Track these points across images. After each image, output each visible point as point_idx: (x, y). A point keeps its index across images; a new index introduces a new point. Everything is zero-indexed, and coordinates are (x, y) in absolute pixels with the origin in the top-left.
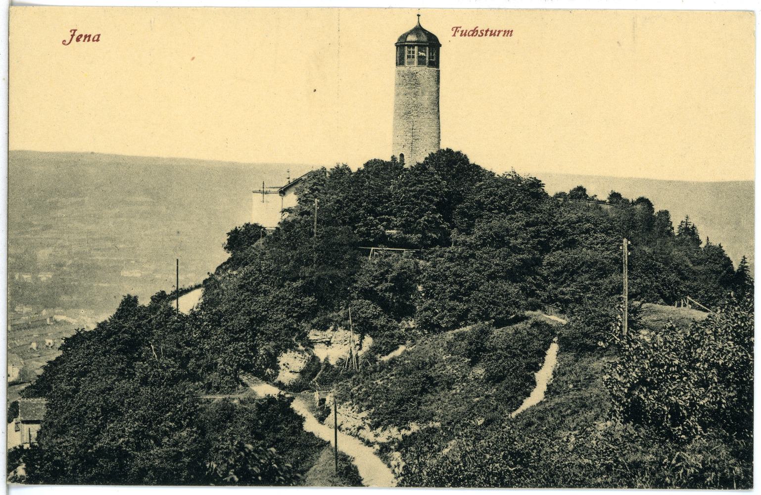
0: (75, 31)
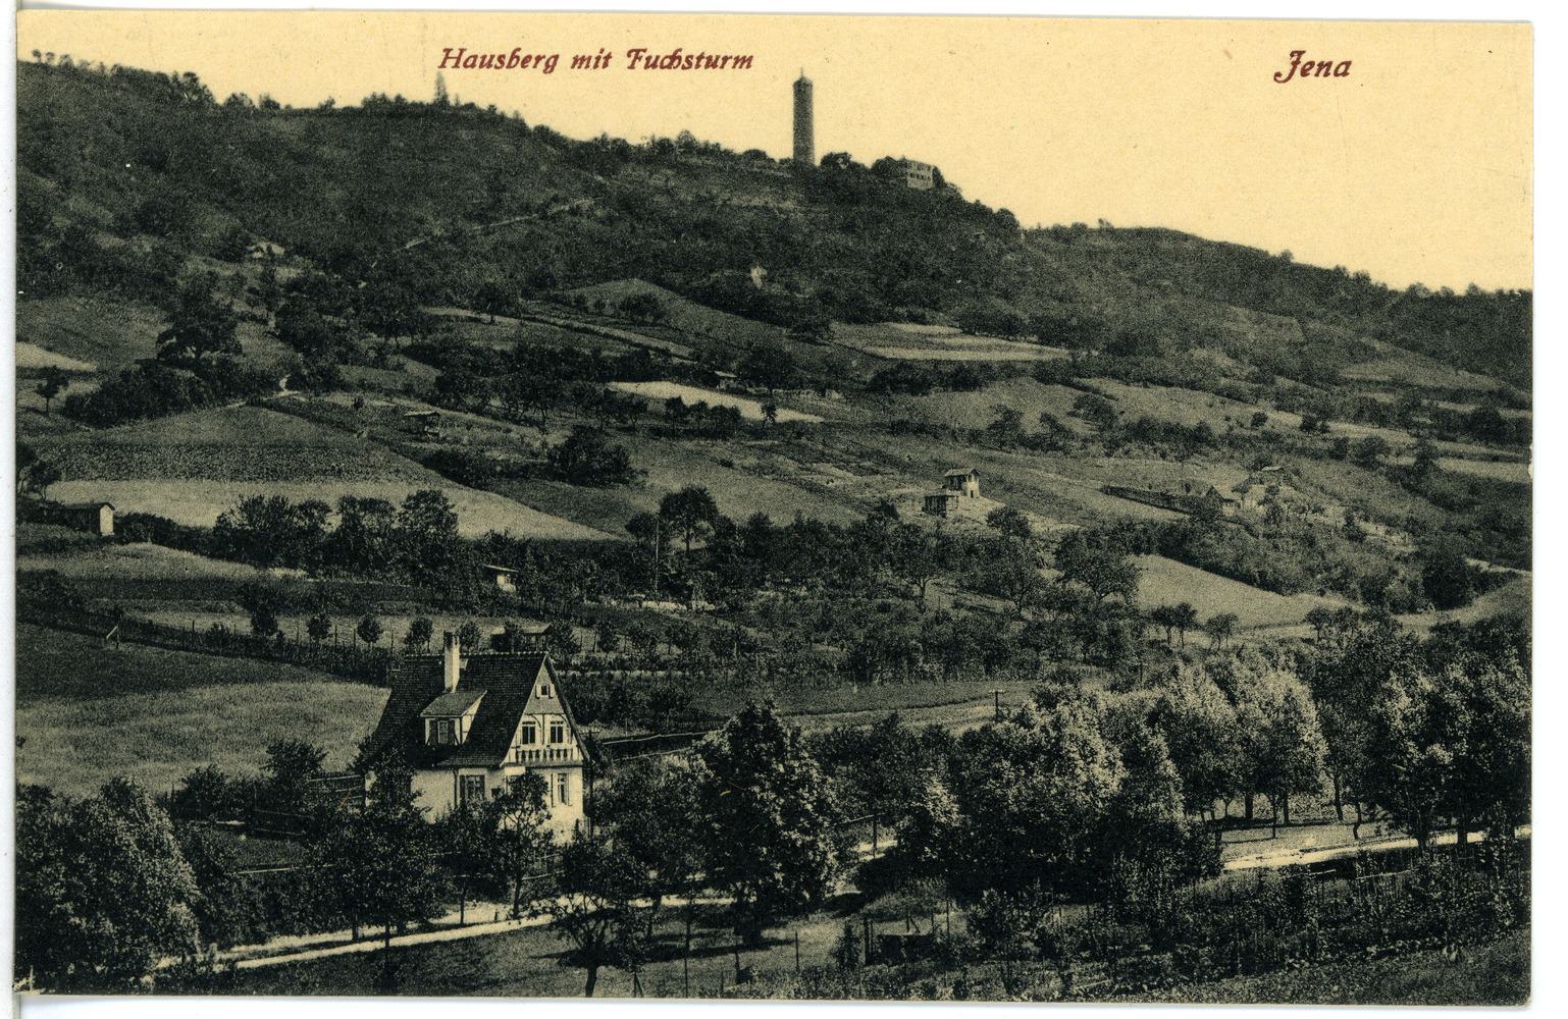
0: (1300, 53)
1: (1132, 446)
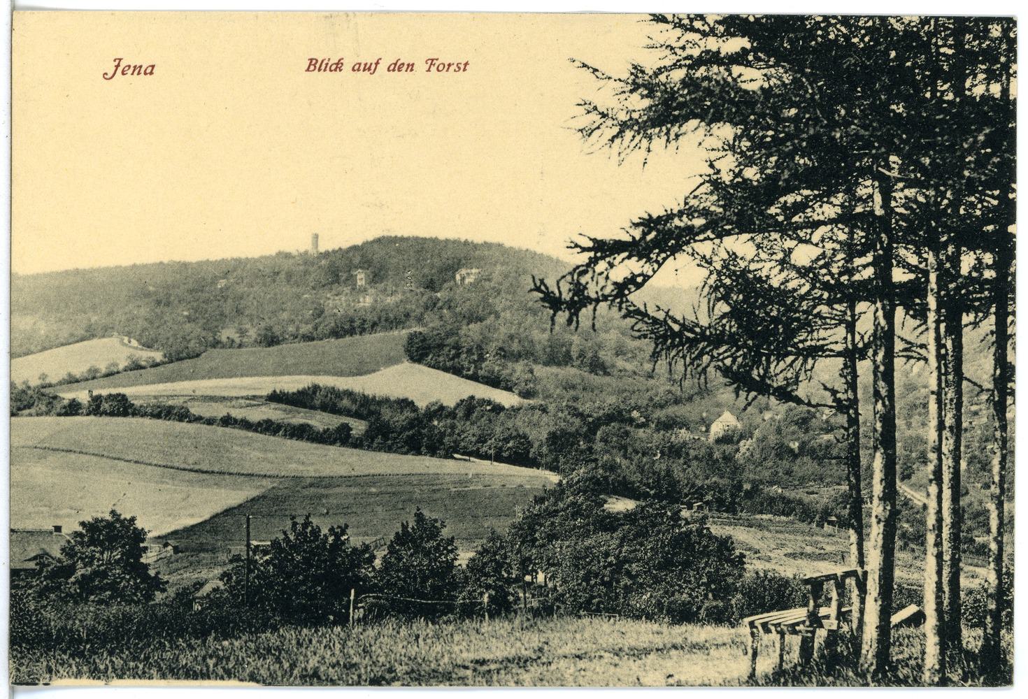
0: (120, 60)
1: (1008, 415)
